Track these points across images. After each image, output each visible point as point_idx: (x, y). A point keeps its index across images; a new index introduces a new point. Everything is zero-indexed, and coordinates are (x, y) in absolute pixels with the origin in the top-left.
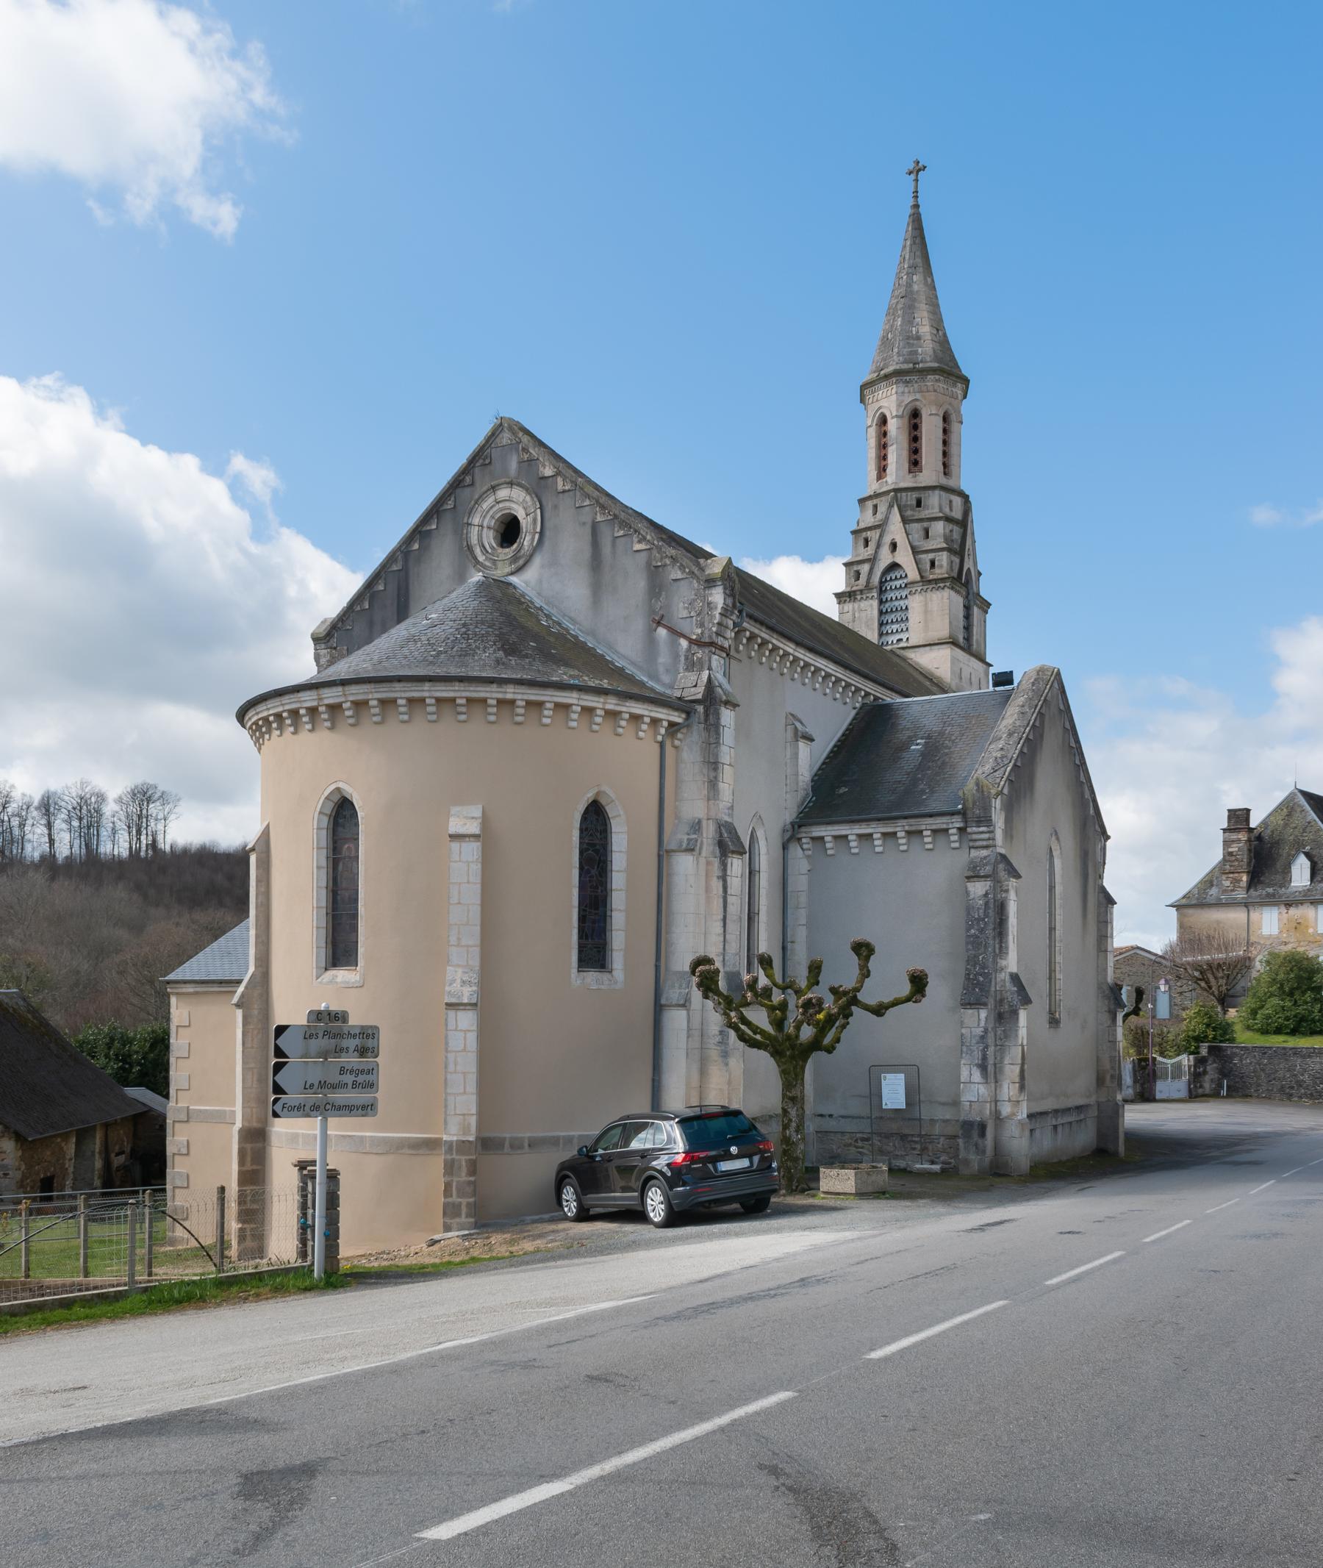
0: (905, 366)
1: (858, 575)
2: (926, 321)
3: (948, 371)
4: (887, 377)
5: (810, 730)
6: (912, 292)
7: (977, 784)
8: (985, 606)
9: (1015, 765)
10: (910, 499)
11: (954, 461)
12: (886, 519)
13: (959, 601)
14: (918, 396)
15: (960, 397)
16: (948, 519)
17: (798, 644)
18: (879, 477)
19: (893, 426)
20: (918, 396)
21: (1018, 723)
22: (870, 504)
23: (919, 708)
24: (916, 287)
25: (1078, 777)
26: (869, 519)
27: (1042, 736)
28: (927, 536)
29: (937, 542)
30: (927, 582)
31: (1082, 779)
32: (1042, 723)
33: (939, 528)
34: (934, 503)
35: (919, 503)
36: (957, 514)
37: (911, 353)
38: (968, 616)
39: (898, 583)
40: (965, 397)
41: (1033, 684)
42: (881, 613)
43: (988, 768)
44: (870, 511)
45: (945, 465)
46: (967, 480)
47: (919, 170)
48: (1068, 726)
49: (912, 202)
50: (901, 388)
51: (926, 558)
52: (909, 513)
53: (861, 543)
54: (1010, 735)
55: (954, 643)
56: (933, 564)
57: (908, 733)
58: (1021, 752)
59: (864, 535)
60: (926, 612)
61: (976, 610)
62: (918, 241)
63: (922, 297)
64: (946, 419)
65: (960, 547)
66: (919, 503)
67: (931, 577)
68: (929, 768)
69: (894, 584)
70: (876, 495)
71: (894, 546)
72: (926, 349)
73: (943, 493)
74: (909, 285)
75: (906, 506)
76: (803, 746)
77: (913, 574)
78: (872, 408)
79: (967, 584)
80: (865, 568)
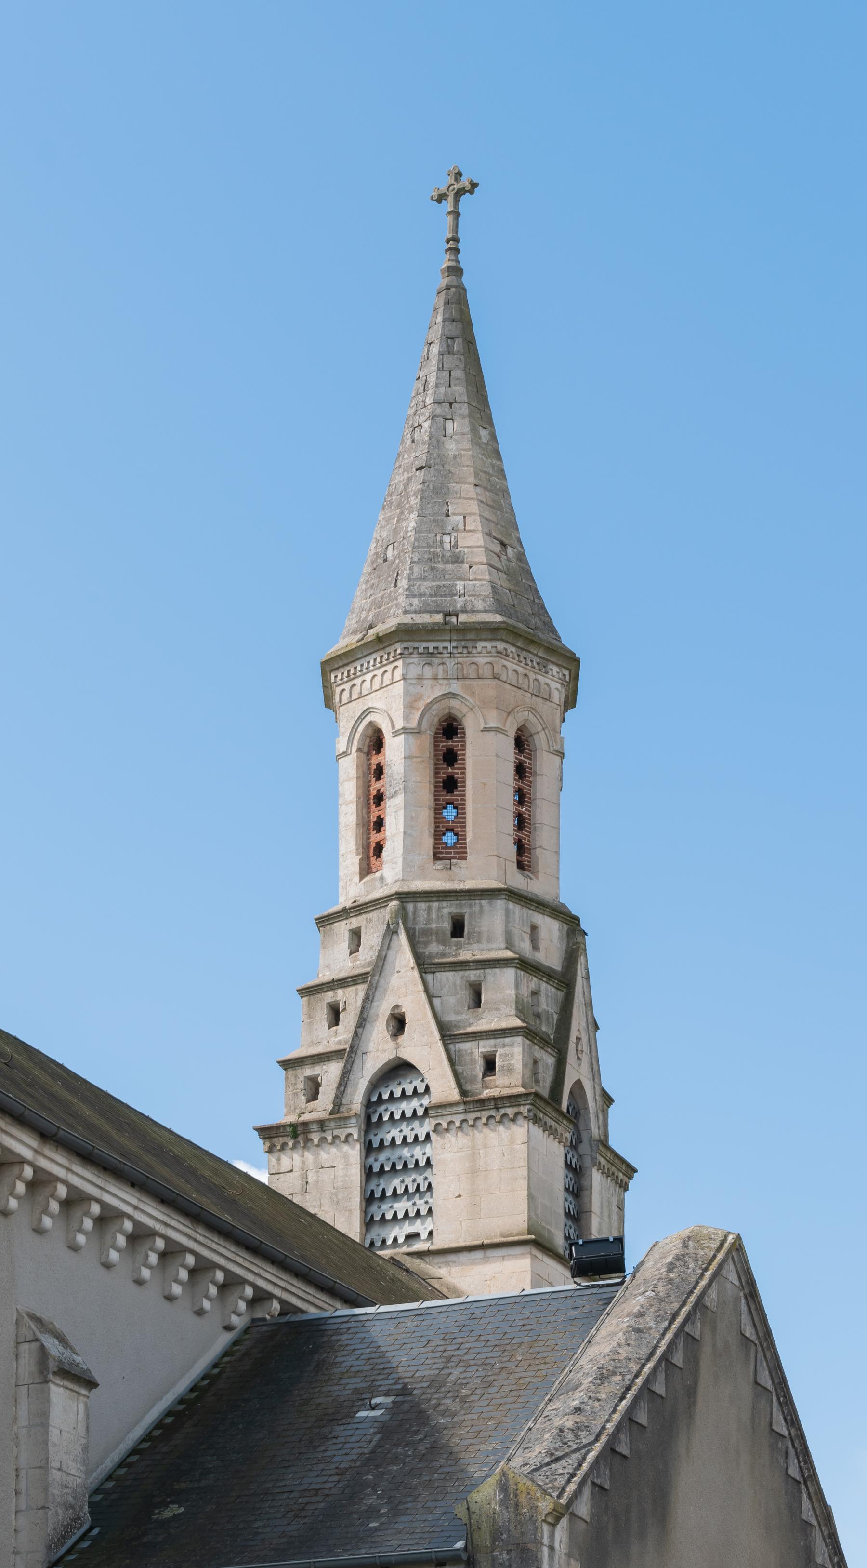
0: (425, 619)
1: (313, 1088)
2: (474, 523)
3: (526, 631)
4: (381, 642)
5: (84, 1360)
6: (442, 459)
7: (504, 1487)
8: (622, 1172)
9: (610, 1450)
10: (439, 917)
11: (542, 838)
12: (381, 962)
13: (555, 1153)
14: (456, 687)
15: (558, 696)
16: (526, 965)
17: (46, 1136)
18: (366, 870)
19: (395, 753)
20: (456, 687)
21: (624, 1352)
22: (343, 928)
23: (391, 1327)
24: (451, 447)
25: (795, 1509)
26: (337, 960)
27: (691, 1392)
28: (477, 1001)
29: (500, 1013)
30: (478, 1107)
31: (808, 1514)
32: (693, 1359)
33: (503, 986)
34: (494, 930)
35: (458, 929)
36: (551, 955)
37: (437, 592)
38: (577, 1191)
39: (407, 1107)
40: (570, 702)
41: (671, 1267)
42: (369, 1174)
43: (537, 1453)
44: (344, 944)
45: (521, 848)
46: (573, 876)
47: (459, 193)
48: (766, 1380)
49: (445, 261)
50: (416, 665)
51: (476, 1050)
52: (433, 948)
53: (322, 1014)
54: (602, 1377)
55: (538, 1243)
56: (490, 1066)
57: (356, 1383)
58: (629, 1419)
59: (329, 997)
60: (473, 1172)
61: (597, 1180)
62: (457, 346)
63: (467, 471)
64: (521, 743)
65: (556, 1024)
66: (458, 929)
67: (486, 1093)
68: (396, 1459)
69: (398, 1108)
70: (359, 909)
71: (398, 1023)
72: (475, 591)
73: (516, 909)
74: (436, 441)
75: (427, 932)
76: (59, 1394)
77: (442, 1086)
78: (348, 715)
79: (575, 1115)
80: (330, 1073)
